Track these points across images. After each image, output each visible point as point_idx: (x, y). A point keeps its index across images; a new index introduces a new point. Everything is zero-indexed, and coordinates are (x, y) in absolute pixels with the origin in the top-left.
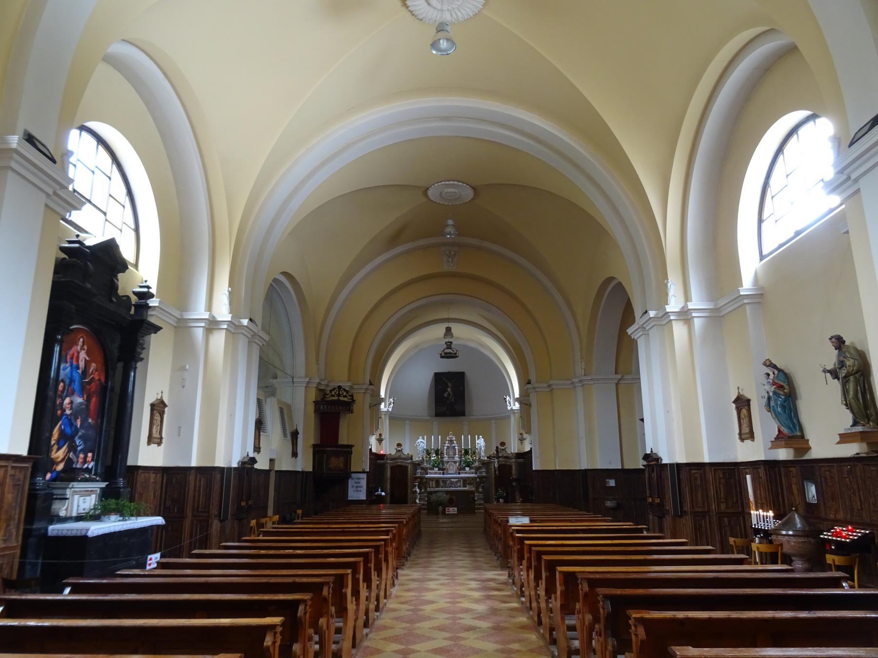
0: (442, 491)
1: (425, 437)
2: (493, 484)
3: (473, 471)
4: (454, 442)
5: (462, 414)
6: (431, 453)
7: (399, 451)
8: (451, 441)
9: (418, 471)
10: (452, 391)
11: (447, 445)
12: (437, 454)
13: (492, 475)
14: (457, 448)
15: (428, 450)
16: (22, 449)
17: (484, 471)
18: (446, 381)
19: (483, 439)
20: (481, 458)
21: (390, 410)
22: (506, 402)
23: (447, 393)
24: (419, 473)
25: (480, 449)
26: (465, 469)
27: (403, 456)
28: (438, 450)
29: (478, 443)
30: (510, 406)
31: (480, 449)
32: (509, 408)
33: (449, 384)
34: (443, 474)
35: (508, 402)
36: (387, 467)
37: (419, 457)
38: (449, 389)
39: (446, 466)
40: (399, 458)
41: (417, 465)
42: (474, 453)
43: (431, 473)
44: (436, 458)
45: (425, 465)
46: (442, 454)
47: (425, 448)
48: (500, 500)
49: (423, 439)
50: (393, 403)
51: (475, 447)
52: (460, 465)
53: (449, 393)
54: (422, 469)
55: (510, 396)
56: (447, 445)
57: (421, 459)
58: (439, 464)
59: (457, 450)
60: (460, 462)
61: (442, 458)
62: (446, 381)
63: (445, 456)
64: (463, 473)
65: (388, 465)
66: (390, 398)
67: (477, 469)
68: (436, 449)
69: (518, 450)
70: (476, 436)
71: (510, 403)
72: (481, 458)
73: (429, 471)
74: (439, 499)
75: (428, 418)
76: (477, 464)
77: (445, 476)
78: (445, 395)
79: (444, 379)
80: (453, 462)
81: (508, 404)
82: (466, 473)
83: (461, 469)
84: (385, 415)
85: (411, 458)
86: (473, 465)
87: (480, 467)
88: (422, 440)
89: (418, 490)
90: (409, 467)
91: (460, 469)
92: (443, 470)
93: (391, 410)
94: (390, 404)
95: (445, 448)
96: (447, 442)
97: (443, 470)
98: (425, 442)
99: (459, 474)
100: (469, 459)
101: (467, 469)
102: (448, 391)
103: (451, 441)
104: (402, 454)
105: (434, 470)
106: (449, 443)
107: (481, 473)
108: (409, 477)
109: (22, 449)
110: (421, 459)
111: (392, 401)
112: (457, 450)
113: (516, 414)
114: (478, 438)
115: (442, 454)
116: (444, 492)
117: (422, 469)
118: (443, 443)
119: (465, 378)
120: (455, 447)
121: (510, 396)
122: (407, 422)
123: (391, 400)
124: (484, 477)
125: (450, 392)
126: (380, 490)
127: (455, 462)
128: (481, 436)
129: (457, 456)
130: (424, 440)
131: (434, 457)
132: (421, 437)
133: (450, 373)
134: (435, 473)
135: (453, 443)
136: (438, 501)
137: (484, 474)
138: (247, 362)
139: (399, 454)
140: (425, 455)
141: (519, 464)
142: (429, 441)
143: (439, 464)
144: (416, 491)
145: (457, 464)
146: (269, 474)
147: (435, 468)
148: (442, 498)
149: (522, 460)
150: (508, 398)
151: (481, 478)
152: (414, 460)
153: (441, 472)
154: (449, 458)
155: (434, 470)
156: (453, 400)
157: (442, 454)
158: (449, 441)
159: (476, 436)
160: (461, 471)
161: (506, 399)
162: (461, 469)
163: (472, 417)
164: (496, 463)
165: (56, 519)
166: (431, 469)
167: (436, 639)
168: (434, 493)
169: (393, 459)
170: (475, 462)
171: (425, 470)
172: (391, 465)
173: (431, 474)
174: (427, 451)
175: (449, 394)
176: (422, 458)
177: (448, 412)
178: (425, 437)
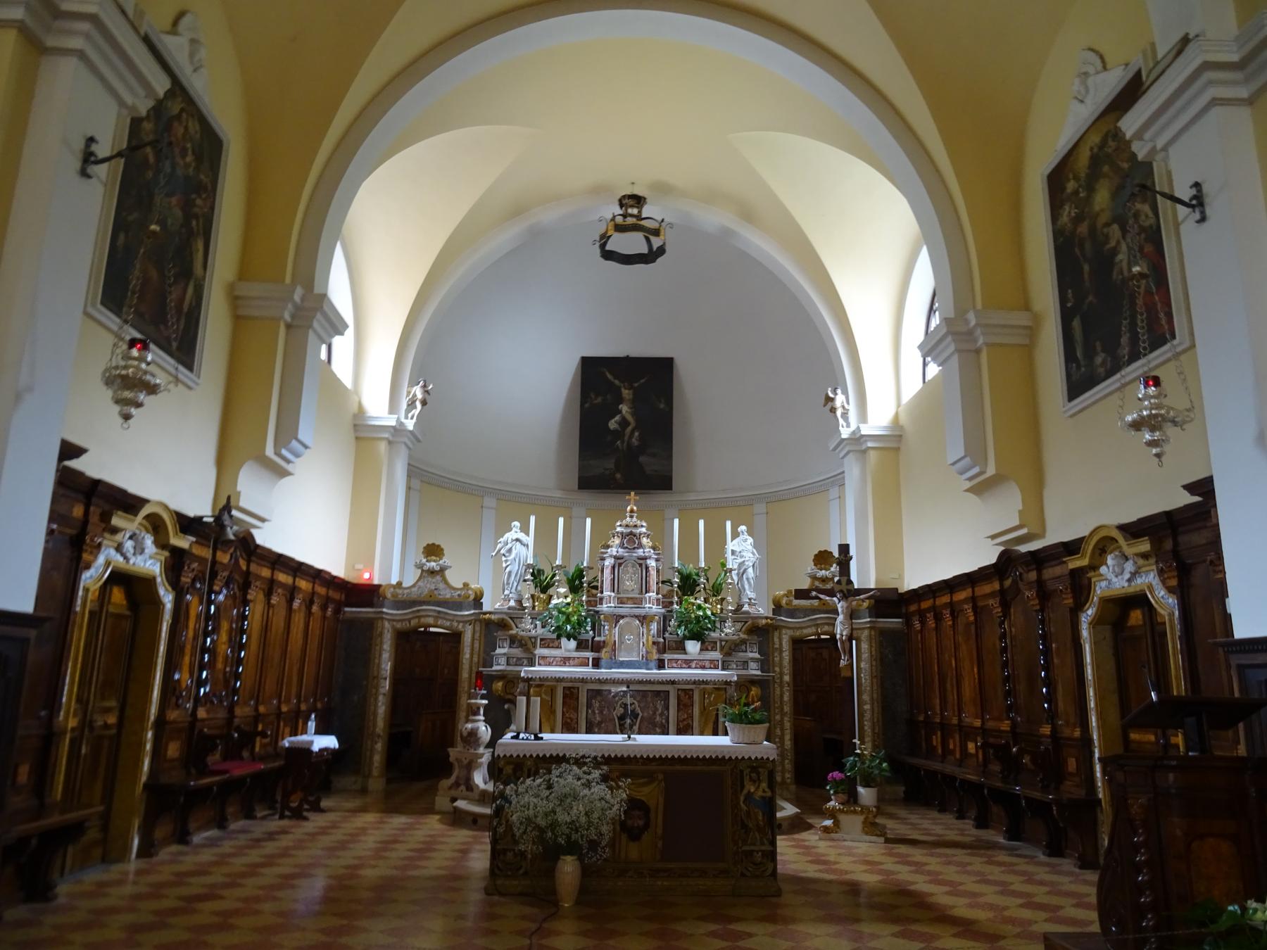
0: (580, 762)
1: (533, 519)
2: (787, 709)
3: (716, 655)
4: (645, 541)
5: (661, 482)
6: (549, 586)
7: (432, 572)
8: (631, 539)
9: (499, 651)
10: (633, 414)
11: (613, 551)
12: (575, 588)
13: (782, 674)
14: (652, 563)
15: (540, 572)
16: (25, 603)
17: (753, 659)
18: (617, 382)
19: (750, 540)
20: (746, 608)
21: (410, 424)
22: (833, 410)
23: (617, 418)
24: (503, 660)
25: (741, 576)
26: (683, 649)
27: (447, 594)
28: (580, 574)
29: (733, 552)
30: (848, 426)
31: (741, 576)
32: (845, 433)
33: (626, 393)
34: (596, 664)
35: (839, 413)
36: (381, 634)
37: (507, 599)
38: (624, 408)
39: (610, 633)
40: (432, 600)
41: (495, 628)
42: (717, 590)
43: (545, 660)
44: (569, 600)
45: (528, 627)
46: (595, 587)
47: (530, 561)
48: (861, 790)
49: (525, 529)
50: (424, 403)
51: (724, 565)
52: (663, 630)
53: (624, 419)
54: (513, 641)
55: (845, 392)
56: (613, 551)
57: (512, 603)
58: (580, 624)
59: (653, 573)
60: (666, 619)
61: (595, 601)
62: (617, 382)
63: (606, 593)
64: (675, 663)
65: (387, 624)
66: (413, 383)
67: (731, 649)
68: (572, 570)
69: (877, 582)
70: (729, 524)
71: (845, 415)
72: (746, 608)
73: (540, 651)
74: (562, 817)
75: (558, 494)
76: (729, 629)
77: (603, 672)
78: (613, 424)
79: (609, 376)
80: (637, 617)
81: (841, 421)
82: (688, 664)
83: (668, 647)
84: (390, 443)
85: (477, 602)
86: (713, 634)
87: (743, 642)
88: (522, 536)
89: (484, 731)
90: (467, 638)
91: (662, 650)
92: (597, 647)
93: (411, 427)
94: (411, 405)
95: (609, 562)
96: (617, 541)
97: (597, 647)
98: (530, 540)
99: (661, 665)
100: (699, 607)
101: (693, 647)
102: (620, 412)
103: (631, 539)
104: (441, 586)
105: (559, 647)
106: (622, 545)
107: (745, 664)
108: (465, 674)
109: (25, 603)
110: (512, 603)
111: (419, 396)
112: (653, 573)
113: (872, 454)
114: (735, 535)
115: (596, 588)
116: (608, 760)
117: (513, 641)
118: (601, 544)
119: (674, 366)
120: (645, 558)
121: (845, 392)
122: (490, 502)
123: (418, 392)
124: (753, 681)
125: (629, 418)
126: (312, 725)
127: (644, 619)
128: (743, 528)
129: (653, 595)
130: (527, 534)
131: (561, 596)
132: (517, 524)
133: (627, 359)
134: (565, 661)
135: (641, 546)
136: (554, 825)
137: (754, 671)
138: (352, 513)
139: (429, 584)
140: (528, 590)
141: (884, 639)
142: (545, 538)
143: (580, 624)
144: (473, 734)
145: (654, 627)
146: (682, 650)
147: (564, 641)
148: (579, 809)
149: (894, 622)
150: (840, 399)
151: (745, 684)
152: (486, 608)
153: (589, 655)
154: (621, 601)
155: (559, 647)
156: (635, 442)
157: (596, 588)
158: (623, 536)
159: (729, 524)
160: (667, 656)
161: (832, 400)
162: (668, 647)
163: (692, 497)
164: (841, 618)
165: (771, 629)
166: (546, 643)
167: (611, 236)
168: (533, 773)
169: (401, 604)
170: (723, 621)
171: (526, 645)
172: (399, 626)
173: (550, 664)
174: (537, 574)
175: (624, 423)
176: (519, 602)
177: (618, 476)
178: (533, 519)
